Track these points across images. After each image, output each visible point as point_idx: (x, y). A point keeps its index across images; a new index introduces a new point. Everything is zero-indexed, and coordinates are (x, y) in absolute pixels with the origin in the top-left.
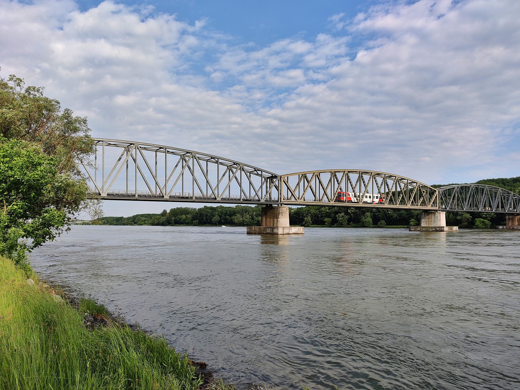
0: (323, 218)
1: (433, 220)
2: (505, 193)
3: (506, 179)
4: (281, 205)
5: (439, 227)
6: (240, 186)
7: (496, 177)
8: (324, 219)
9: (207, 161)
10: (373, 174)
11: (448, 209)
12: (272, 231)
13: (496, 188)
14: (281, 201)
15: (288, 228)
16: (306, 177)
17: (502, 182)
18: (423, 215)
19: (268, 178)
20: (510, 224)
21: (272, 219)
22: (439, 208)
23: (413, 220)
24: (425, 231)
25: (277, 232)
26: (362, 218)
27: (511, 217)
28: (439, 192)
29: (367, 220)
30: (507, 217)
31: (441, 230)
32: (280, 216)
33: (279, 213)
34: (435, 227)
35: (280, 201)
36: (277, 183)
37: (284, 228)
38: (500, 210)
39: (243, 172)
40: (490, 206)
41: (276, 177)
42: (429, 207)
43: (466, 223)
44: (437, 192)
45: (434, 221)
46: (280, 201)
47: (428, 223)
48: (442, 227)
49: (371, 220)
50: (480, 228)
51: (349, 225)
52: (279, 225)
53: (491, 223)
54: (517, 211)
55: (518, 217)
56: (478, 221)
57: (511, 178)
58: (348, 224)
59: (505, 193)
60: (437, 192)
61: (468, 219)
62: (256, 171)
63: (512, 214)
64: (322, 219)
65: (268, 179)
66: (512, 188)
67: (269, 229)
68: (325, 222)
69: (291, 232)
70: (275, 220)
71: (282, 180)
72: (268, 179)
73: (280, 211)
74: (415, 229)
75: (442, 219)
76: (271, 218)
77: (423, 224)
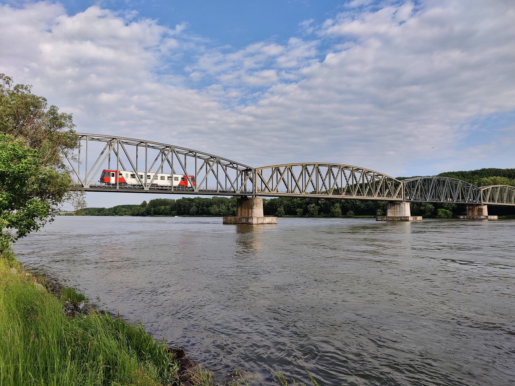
0: (295, 209)
1: (398, 210)
2: (464, 185)
3: (465, 172)
4: (256, 197)
5: (404, 217)
6: (217, 179)
7: (456, 170)
8: (296, 210)
9: (186, 155)
10: (341, 167)
11: (412, 200)
12: (247, 222)
13: (456, 180)
14: (255, 193)
15: (262, 218)
16: (279, 170)
17: (462, 175)
18: (389, 206)
19: (243, 171)
20: (470, 214)
21: (247, 210)
22: (404, 199)
23: (380, 210)
24: (391, 221)
25: (252, 222)
26: (332, 208)
27: (471, 207)
28: (403, 184)
29: (336, 210)
30: (467, 208)
31: (406, 219)
32: (255, 207)
33: (254, 204)
34: (401, 217)
35: (254, 193)
36: (251, 176)
37: (258, 218)
38: (461, 201)
39: (219, 165)
40: (451, 197)
41: (250, 170)
42: (394, 198)
43: (429, 213)
44: (402, 184)
45: (400, 211)
46: (254, 193)
47: (393, 213)
48: (407, 217)
49: (340, 210)
50: (443, 218)
51: (320, 215)
52: (254, 215)
53: (452, 213)
54: (476, 202)
55: (477, 207)
56: (440, 211)
57: (470, 171)
58: (319, 214)
59: (464, 185)
60: (402, 184)
61: (431, 210)
62: (232, 164)
63: (472, 205)
64: (294, 210)
65: (243, 172)
66: (471, 180)
67: (244, 219)
68: (297, 212)
69: (264, 222)
70: (250, 210)
71: (256, 173)
72: (243, 172)
73: (255, 202)
74: (382, 219)
75: (406, 210)
76: (246, 209)
77: (389, 214)
